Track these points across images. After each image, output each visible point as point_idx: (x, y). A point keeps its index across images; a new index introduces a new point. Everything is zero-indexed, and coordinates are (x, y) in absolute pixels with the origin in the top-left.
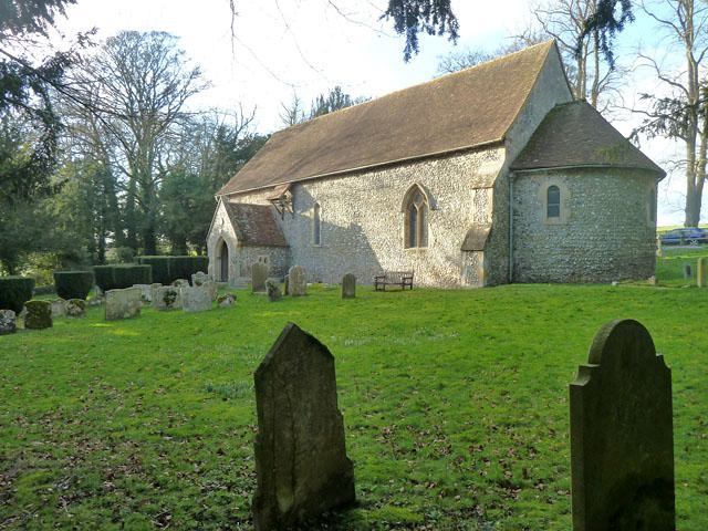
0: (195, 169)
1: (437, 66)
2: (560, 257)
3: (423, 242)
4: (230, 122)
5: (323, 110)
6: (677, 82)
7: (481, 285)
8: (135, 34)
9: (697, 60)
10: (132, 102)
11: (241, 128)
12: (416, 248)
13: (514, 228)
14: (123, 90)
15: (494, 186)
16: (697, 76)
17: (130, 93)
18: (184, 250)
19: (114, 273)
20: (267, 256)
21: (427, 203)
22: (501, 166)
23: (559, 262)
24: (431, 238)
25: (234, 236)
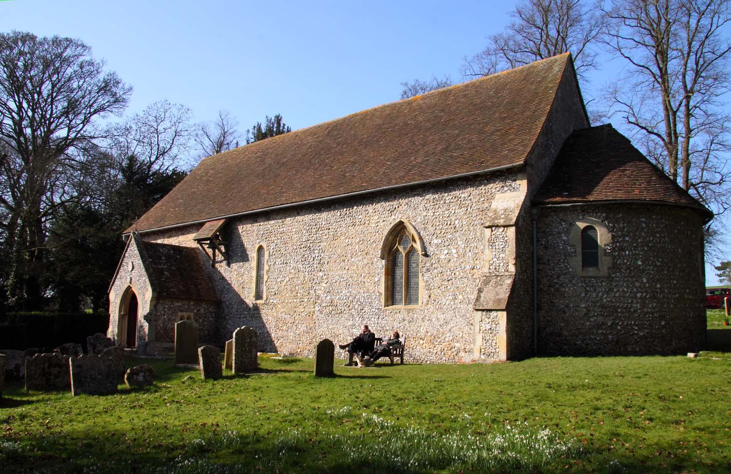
0: (98, 206)
1: (401, 92)
2: (600, 319)
3: (410, 298)
4: (142, 153)
5: (260, 135)
6: (655, 131)
7: (503, 355)
8: (33, 38)
9: (675, 110)
10: (22, 119)
11: (157, 158)
12: (401, 306)
13: (539, 280)
14: (12, 105)
15: (516, 224)
16: (675, 125)
17: (20, 107)
18: (76, 304)
19: (416, 280)
20: (192, 314)
21: (418, 246)
22: (522, 198)
23: (599, 326)
24: (423, 294)
25: (195, 234)
